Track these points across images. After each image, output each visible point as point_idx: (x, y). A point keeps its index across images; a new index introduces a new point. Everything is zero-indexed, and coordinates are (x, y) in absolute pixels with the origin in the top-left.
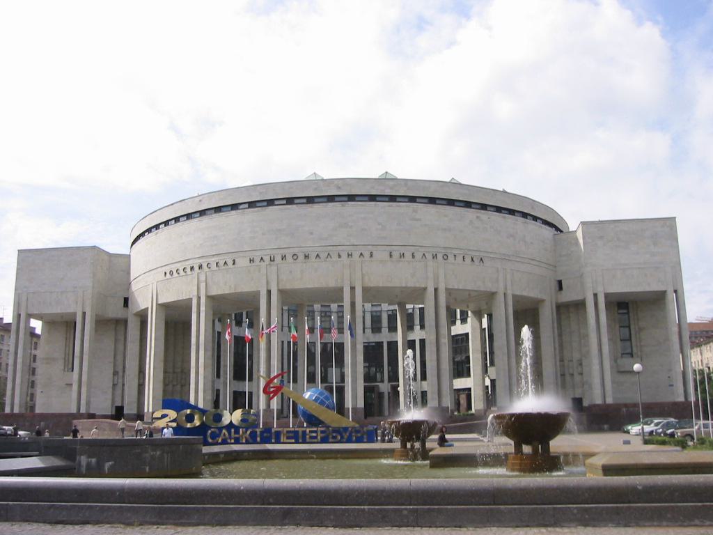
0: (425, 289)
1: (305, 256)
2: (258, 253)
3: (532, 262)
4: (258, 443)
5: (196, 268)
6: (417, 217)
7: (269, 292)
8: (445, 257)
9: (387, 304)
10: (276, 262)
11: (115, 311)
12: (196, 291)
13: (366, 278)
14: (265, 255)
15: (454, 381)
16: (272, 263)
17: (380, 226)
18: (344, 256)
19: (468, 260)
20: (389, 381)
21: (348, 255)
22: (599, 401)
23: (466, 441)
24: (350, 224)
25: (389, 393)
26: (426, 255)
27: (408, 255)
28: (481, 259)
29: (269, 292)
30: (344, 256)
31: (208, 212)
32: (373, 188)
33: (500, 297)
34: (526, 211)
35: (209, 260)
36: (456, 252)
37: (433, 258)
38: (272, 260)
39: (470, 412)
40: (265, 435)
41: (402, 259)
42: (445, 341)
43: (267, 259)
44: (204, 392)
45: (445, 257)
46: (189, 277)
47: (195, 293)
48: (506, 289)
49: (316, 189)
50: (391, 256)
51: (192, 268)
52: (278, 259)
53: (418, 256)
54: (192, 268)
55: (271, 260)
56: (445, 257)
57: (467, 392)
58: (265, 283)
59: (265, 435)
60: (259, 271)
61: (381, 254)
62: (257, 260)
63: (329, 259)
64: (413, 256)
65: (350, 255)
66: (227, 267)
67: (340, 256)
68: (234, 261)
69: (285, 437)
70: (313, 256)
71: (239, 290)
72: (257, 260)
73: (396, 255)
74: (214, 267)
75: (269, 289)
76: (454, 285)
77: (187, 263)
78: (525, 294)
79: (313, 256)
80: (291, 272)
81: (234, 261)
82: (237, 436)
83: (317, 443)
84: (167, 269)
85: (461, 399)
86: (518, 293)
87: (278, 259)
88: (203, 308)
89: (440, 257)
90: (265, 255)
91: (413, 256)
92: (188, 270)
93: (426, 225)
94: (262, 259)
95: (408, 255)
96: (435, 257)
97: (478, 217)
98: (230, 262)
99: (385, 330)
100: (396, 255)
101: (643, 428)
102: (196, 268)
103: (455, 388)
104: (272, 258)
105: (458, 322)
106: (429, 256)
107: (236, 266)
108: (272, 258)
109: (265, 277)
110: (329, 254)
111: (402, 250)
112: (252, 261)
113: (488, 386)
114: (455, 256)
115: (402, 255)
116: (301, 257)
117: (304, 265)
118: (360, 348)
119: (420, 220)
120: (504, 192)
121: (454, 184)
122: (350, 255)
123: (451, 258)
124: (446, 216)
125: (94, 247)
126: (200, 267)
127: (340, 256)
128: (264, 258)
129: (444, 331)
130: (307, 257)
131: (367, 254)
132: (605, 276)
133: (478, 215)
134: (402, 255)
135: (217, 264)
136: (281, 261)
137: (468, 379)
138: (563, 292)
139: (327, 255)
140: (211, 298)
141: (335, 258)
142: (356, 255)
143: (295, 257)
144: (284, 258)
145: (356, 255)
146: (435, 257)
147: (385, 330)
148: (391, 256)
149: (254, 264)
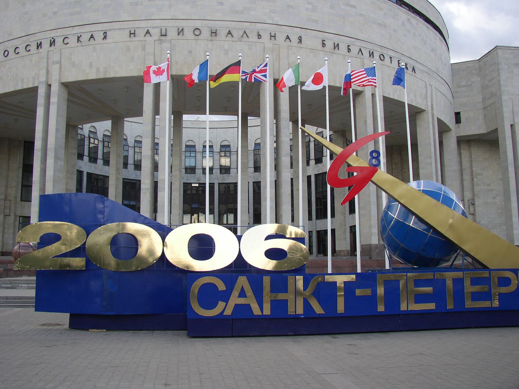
2: (143, 24)
5: (46, 45)
9: (64, 318)
10: (168, 38)
12: (45, 75)
16: (163, 38)
17: (310, 6)
18: (266, 37)
27: (343, 47)
30: (266, 37)
33: (42, 92)
36: (392, 54)
40: (358, 292)
41: (336, 51)
43: (155, 33)
47: (43, 79)
50: (324, 45)
51: (39, 46)
52: (172, 34)
53: (355, 50)
56: (382, 57)
59: (358, 292)
60: (144, 49)
61: (312, 41)
62: (141, 33)
64: (349, 50)
66: (94, 42)
69: (412, 298)
70: (223, 33)
72: (141, 33)
73: (329, 45)
74: (72, 41)
76: (72, 77)
77: (32, 38)
79: (223, 33)
80: (190, 52)
82: (281, 296)
87: (172, 34)
88: (54, 99)
91: (349, 50)
93: (361, 15)
94: (148, 32)
95: (343, 47)
98: (99, 36)
100: (329, 45)
102: (46, 45)
106: (366, 54)
107: (108, 40)
109: (152, 57)
111: (337, 39)
112: (132, 34)
115: (336, 46)
116: (206, 33)
117: (210, 44)
119: (354, 7)
122: (273, 37)
123: (387, 59)
124: (381, 9)
125: (80, 322)
126: (52, 43)
128: (151, 31)
130: (214, 33)
131: (294, 39)
134: (336, 46)
135: (79, 38)
136: (129, 39)
138: (461, 124)
139: (241, 33)
141: (253, 38)
142: (281, 38)
143: (197, 32)
144: (180, 32)
145: (281, 38)
148: (324, 45)
149: (136, 39)
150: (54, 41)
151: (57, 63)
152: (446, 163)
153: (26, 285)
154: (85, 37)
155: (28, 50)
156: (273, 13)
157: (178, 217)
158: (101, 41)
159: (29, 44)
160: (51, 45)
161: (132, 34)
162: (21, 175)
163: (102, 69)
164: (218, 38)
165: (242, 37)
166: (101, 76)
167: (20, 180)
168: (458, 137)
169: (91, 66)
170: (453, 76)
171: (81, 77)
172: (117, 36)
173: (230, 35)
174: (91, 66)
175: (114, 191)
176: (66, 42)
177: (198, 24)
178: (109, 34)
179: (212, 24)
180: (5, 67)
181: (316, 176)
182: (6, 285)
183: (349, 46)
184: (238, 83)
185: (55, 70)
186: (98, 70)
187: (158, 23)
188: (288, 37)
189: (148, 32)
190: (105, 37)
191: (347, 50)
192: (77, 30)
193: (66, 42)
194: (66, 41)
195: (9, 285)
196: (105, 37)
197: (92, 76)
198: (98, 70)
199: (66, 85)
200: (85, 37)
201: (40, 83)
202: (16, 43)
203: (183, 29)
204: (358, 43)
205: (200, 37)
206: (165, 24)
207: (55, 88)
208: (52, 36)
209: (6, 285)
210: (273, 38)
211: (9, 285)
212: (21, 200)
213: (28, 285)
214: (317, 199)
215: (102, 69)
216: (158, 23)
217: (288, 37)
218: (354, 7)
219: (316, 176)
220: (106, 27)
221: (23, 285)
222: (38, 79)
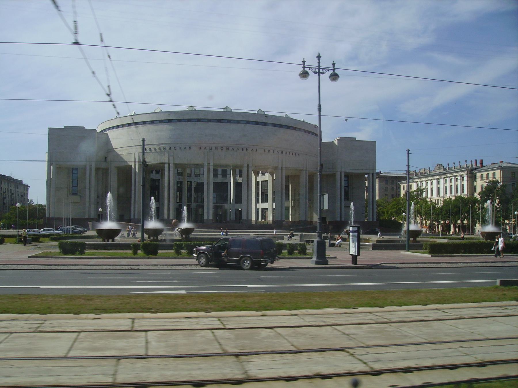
4: (498, 253)
8: (286, 153)
11: (104, 165)
18: (245, 150)
19: (294, 154)
22: (339, 219)
27: (271, 151)
30: (245, 150)
33: (166, 166)
38: (211, 149)
43: (208, 148)
45: (286, 153)
47: (167, 161)
50: (265, 151)
67: (243, 150)
72: (203, 148)
83: (402, 247)
89: (284, 153)
95: (271, 151)
96: (282, 153)
98: (188, 148)
99: (220, 176)
101: (8, 186)
105: (260, 175)
106: (280, 152)
112: (200, 148)
116: (225, 149)
120: (304, 122)
121: (287, 118)
122: (247, 150)
123: (288, 153)
127: (243, 150)
130: (228, 149)
131: (255, 150)
132: (347, 164)
142: (250, 150)
144: (216, 148)
146: (282, 153)
147: (220, 176)
148: (265, 151)
154: (183, 148)
161: (200, 148)
170: (194, 165)
178: (191, 147)
181: (262, 181)
184: (163, 164)
185: (171, 158)
199: (116, 167)
200: (183, 148)
202: (155, 146)
214: (262, 193)
216: (183, 145)
219: (262, 181)
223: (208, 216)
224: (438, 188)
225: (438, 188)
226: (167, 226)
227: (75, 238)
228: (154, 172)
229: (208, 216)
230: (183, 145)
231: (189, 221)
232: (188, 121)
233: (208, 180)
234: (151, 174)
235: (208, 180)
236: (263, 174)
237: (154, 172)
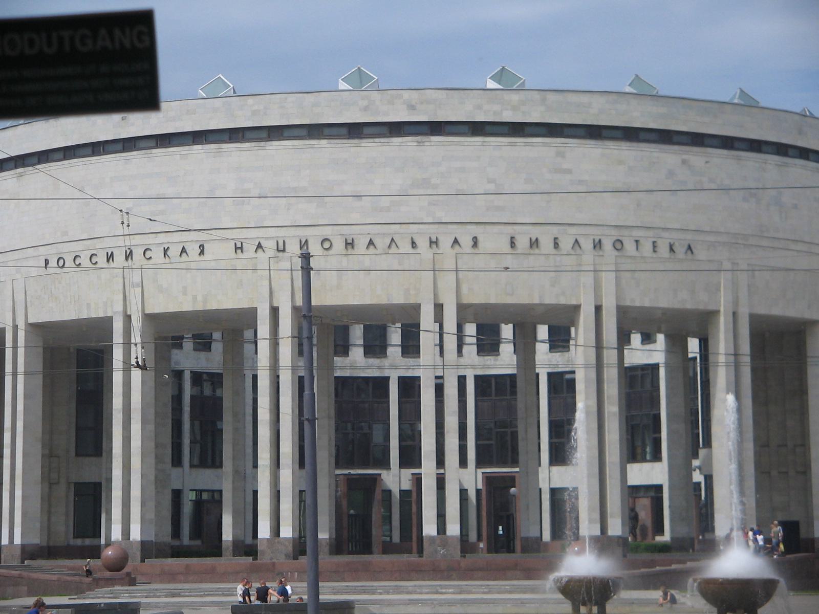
0: (577, 308)
1: (347, 244)
3: (793, 246)
5: (119, 258)
6: (565, 166)
7: (275, 311)
13: (464, 289)
14: (267, 238)
15: (629, 466)
16: (281, 254)
18: (423, 243)
20: (480, 463)
21: (431, 242)
22: (306, 589)
23: (125, 297)
24: (434, 181)
25: (478, 492)
26: (582, 241)
28: (689, 248)
29: (275, 311)
31: (142, 144)
32: (479, 107)
34: (784, 141)
35: (150, 240)
36: (637, 234)
37: (595, 247)
39: (659, 539)
42: (611, 375)
43: (270, 245)
44: (143, 505)
46: (105, 274)
48: (736, 303)
49: (366, 109)
50: (513, 244)
51: (110, 257)
54: (110, 257)
55: (278, 250)
56: (618, 246)
57: (652, 494)
58: (267, 295)
63: (394, 249)
64: (556, 245)
65: (434, 243)
67: (414, 244)
68: (202, 247)
70: (361, 243)
71: (213, 305)
73: (523, 243)
75: (275, 305)
77: (98, 244)
78: (777, 311)
79: (361, 243)
81: (202, 247)
84: (52, 253)
85: (638, 509)
86: (762, 310)
90: (267, 238)
91: (556, 245)
92: (101, 260)
94: (259, 246)
96: (598, 245)
97: (684, 162)
99: (394, 351)
100: (523, 243)
102: (119, 258)
103: (629, 484)
104: (281, 247)
106: (587, 244)
108: (281, 247)
110: (392, 239)
111: (535, 232)
112: (239, 248)
113: (699, 484)
114: (637, 241)
115: (534, 243)
116: (339, 245)
118: (513, 474)
119: (569, 171)
122: (434, 243)
126: (129, 255)
127: (414, 244)
129: (610, 356)
130: (350, 244)
131: (466, 241)
133: (685, 157)
134: (534, 243)
136: (233, 255)
137: (657, 465)
139: (388, 241)
140: (150, 319)
141: (406, 247)
142: (446, 243)
143: (327, 245)
145: (446, 243)
147: (394, 351)
148: (513, 244)
149: (245, 255)
150: (131, 252)
151: (138, 286)
152: (234, 151)
153: (127, 595)
154: (174, 251)
155: (94, 261)
156: (434, 205)
157: (327, 490)
158: (198, 258)
159: (94, 252)
160: (127, 258)
162: (73, 411)
163: (200, 298)
164: (356, 251)
165: (389, 247)
166: (199, 307)
167: (74, 420)
168: (467, 468)
169: (185, 293)
171: (172, 308)
172: (219, 251)
173: (372, 247)
174: (185, 293)
175: (231, 449)
176: (148, 255)
177: (327, 232)
179: (346, 230)
180: (60, 283)
181: (477, 378)
182: (108, 595)
183: (556, 239)
186: (195, 298)
187: (272, 232)
188: (456, 241)
189: (259, 246)
190: (202, 253)
191: (552, 245)
192: (162, 238)
193: (148, 255)
194: (148, 254)
195: (111, 596)
196: (202, 253)
197: (187, 307)
198: (195, 298)
200: (174, 251)
201: (115, 313)
203: (306, 241)
204: (573, 230)
205: (331, 252)
206: (282, 233)
207: (137, 322)
208: (128, 243)
209: (108, 595)
210: (434, 246)
211: (111, 596)
212: (77, 455)
213: (130, 595)
215: (200, 298)
217: (456, 241)
218: (569, 171)
219: (477, 378)
220: (202, 236)
221: (125, 595)
222: (112, 306)
223: (126, 532)
224: (440, 461)
225: (440, 461)
226: (633, 565)
227: (415, 593)
228: (188, 345)
229: (126, 532)
230: (176, 237)
231: (603, 543)
232: (195, 142)
233: (445, 364)
234: (175, 352)
235: (445, 364)
236: (648, 338)
237: (188, 345)
